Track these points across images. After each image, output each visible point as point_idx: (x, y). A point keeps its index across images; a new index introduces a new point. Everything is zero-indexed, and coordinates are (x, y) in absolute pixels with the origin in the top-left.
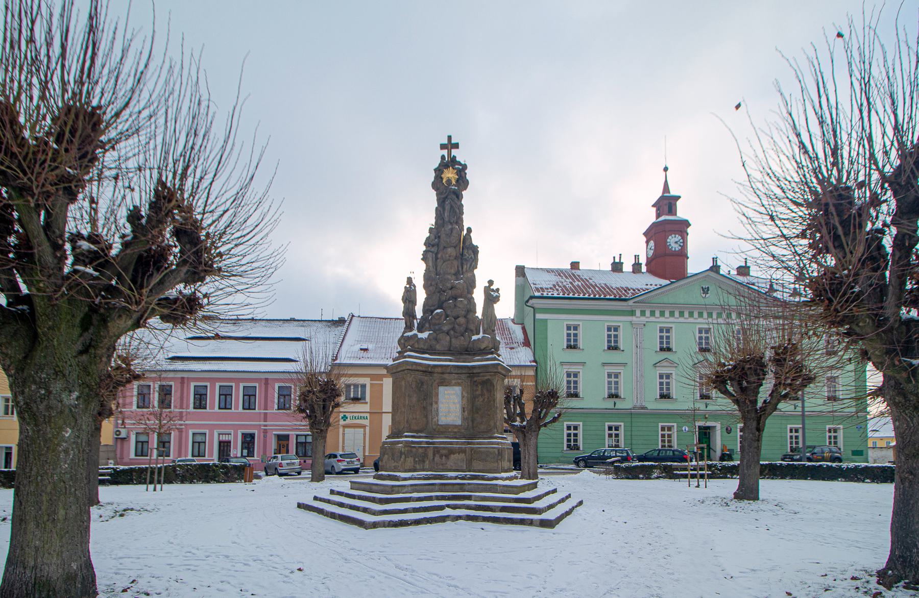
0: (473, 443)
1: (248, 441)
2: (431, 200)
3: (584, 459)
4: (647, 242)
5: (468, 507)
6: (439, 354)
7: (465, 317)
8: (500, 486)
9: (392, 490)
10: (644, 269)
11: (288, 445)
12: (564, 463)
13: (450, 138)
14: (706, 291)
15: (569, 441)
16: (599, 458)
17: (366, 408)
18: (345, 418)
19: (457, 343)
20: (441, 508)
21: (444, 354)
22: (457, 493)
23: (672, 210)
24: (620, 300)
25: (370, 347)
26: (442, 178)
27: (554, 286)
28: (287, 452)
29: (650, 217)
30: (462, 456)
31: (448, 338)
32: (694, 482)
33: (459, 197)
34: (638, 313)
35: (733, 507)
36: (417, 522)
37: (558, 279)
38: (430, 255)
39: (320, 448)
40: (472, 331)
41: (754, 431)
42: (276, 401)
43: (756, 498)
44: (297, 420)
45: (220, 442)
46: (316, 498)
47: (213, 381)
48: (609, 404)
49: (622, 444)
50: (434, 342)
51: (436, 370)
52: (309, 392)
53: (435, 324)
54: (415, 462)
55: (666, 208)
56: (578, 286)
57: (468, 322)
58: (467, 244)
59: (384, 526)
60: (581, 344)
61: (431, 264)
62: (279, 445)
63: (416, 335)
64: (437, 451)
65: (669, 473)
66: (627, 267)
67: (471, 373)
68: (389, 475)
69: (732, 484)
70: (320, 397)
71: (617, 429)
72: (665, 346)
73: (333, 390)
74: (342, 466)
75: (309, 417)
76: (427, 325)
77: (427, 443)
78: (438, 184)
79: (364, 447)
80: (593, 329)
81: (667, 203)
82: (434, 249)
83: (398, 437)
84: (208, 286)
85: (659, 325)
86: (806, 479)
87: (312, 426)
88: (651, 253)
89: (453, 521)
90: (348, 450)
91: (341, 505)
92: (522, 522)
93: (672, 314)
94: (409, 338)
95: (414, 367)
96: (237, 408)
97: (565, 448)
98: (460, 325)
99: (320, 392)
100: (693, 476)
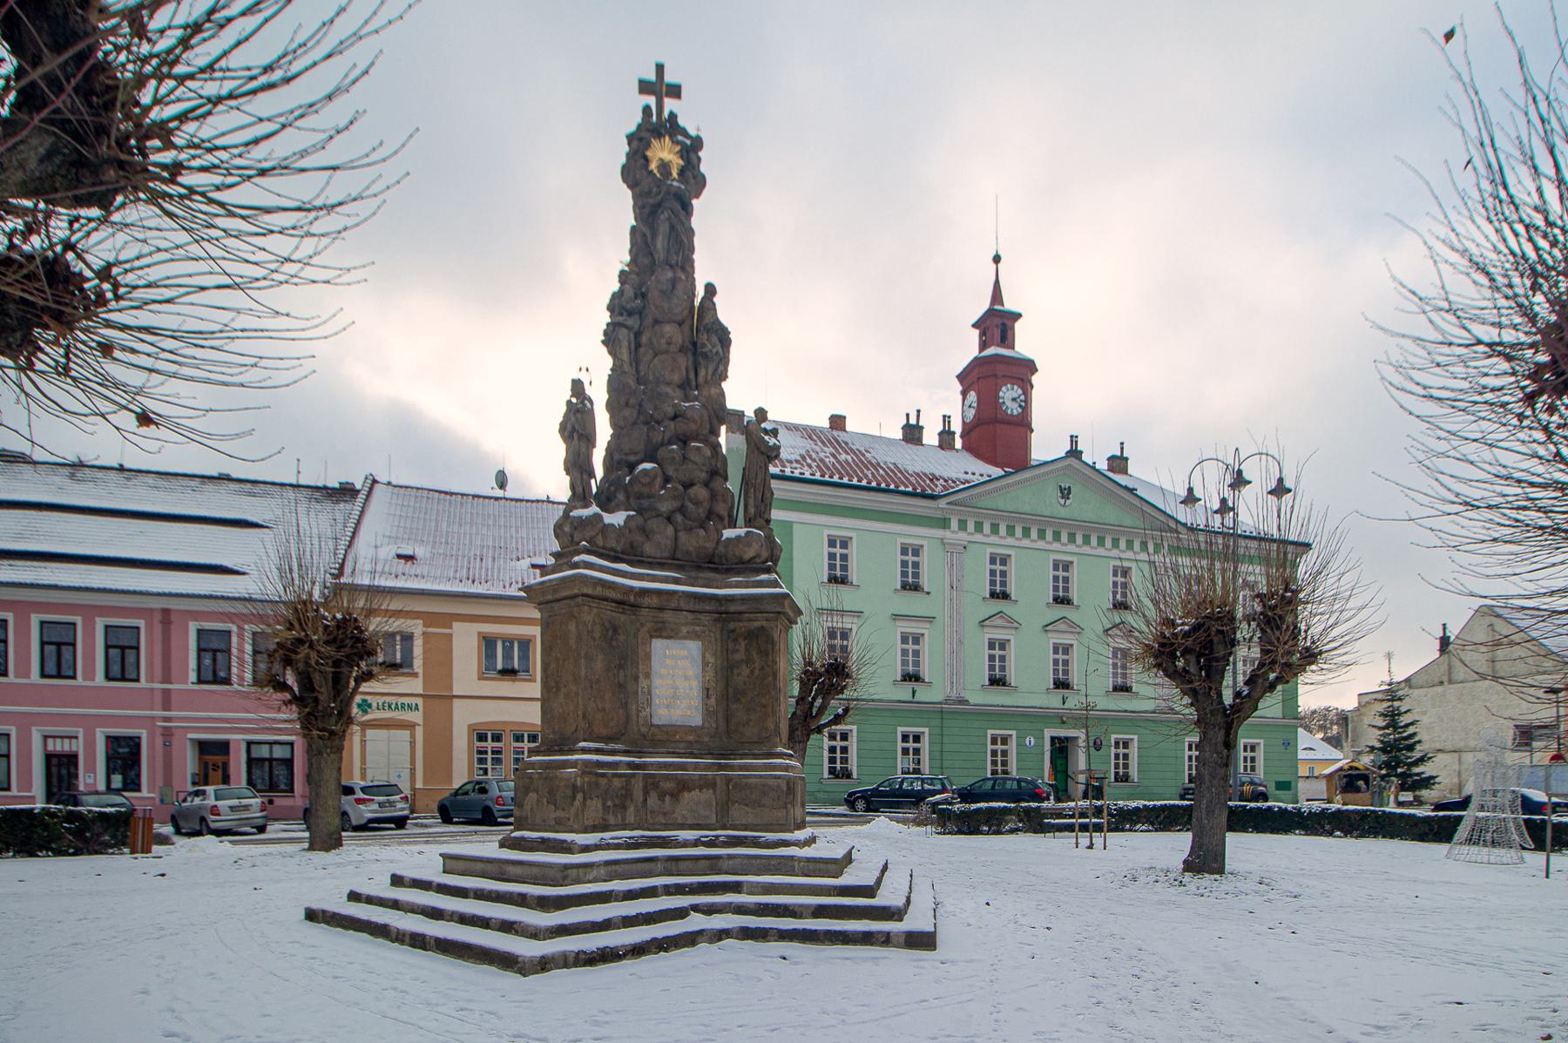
0: (731, 767)
1: (124, 758)
2: (620, 211)
3: (865, 796)
4: (964, 393)
5: (740, 910)
6: (650, 565)
7: (706, 485)
8: (800, 859)
9: (564, 875)
10: (958, 444)
11: (226, 766)
12: (825, 803)
13: (660, 68)
14: (1065, 493)
15: (832, 760)
16: (893, 793)
17: (416, 686)
18: (365, 707)
19: (693, 542)
20: (681, 913)
21: (661, 565)
22: (708, 880)
23: (1006, 338)
24: (924, 496)
25: (420, 552)
26: (646, 159)
27: (803, 458)
28: (226, 779)
29: (968, 348)
30: (707, 794)
31: (670, 530)
32: (1084, 839)
33: (687, 209)
34: (954, 524)
35: (1192, 887)
36: (638, 950)
37: (808, 445)
38: (623, 334)
39: (329, 774)
40: (721, 519)
41: (1221, 747)
42: (193, 664)
43: (1220, 870)
44: (270, 708)
45: (49, 757)
46: (354, 897)
47: (90, 612)
48: (904, 692)
49: (925, 767)
50: (639, 538)
51: (647, 601)
52: (300, 641)
53: (640, 497)
54: (606, 809)
55: (997, 333)
56: (846, 461)
57: (713, 496)
58: (708, 319)
59: (566, 966)
60: (854, 576)
61: (625, 356)
62: (204, 766)
63: (598, 517)
64: (651, 784)
65: (1036, 823)
66: (931, 437)
67: (723, 612)
68: (544, 840)
69: (1178, 844)
70: (326, 654)
71: (917, 739)
72: (998, 589)
73: (358, 640)
74: (368, 811)
75: (298, 700)
76: (621, 497)
77: (630, 765)
78: (635, 171)
79: (413, 770)
80: (876, 549)
81: (997, 324)
82: (633, 322)
83: (562, 752)
84: (109, 240)
85: (990, 550)
86: (1245, 831)
87: (308, 722)
88: (971, 414)
89: (711, 941)
90: (377, 776)
91: (435, 914)
92: (867, 938)
93: (1011, 531)
94: (582, 523)
95: (599, 591)
96: (90, 675)
97: (826, 775)
98: (697, 503)
99: (327, 643)
100: (1084, 828)
